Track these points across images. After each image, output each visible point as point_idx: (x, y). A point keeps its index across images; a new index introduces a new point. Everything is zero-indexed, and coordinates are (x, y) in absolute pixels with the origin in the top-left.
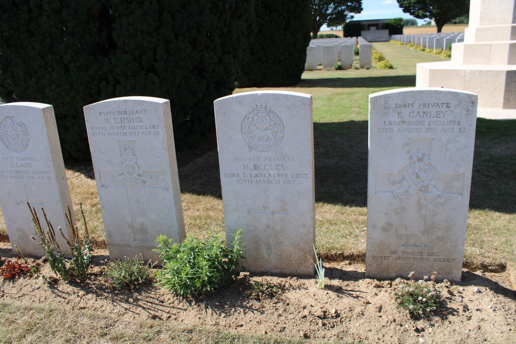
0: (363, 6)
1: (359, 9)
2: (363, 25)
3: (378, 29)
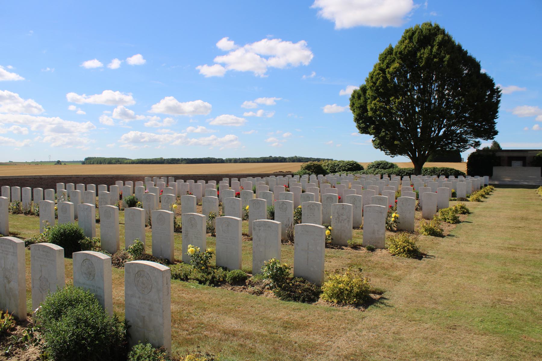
0: (497, 128)
1: (490, 133)
3: (524, 165)
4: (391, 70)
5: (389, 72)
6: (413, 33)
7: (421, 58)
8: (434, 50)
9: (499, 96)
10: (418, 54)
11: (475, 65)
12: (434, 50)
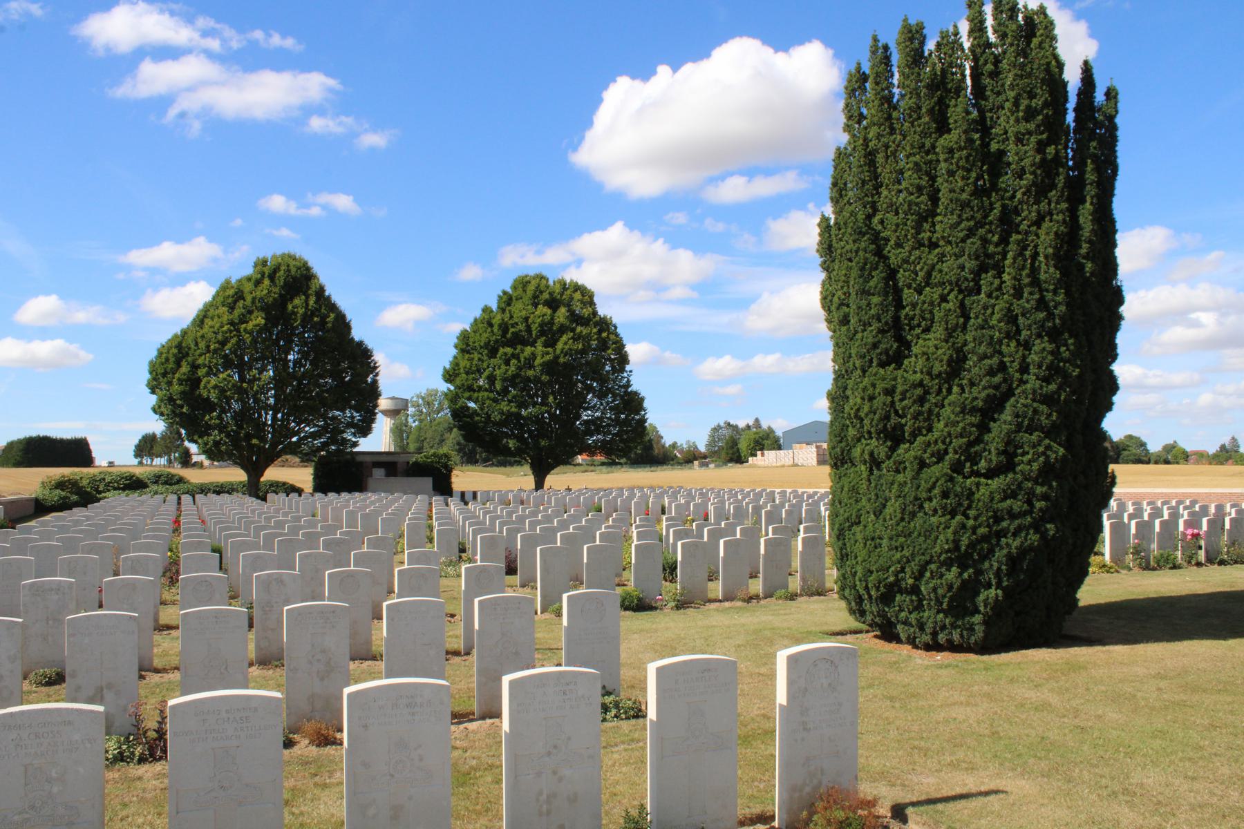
2: (361, 463)
4: (250, 326)
5: (245, 330)
6: (276, 270)
7: (295, 313)
8: (311, 302)
9: (377, 375)
10: (290, 307)
11: (343, 324)
12: (311, 302)
